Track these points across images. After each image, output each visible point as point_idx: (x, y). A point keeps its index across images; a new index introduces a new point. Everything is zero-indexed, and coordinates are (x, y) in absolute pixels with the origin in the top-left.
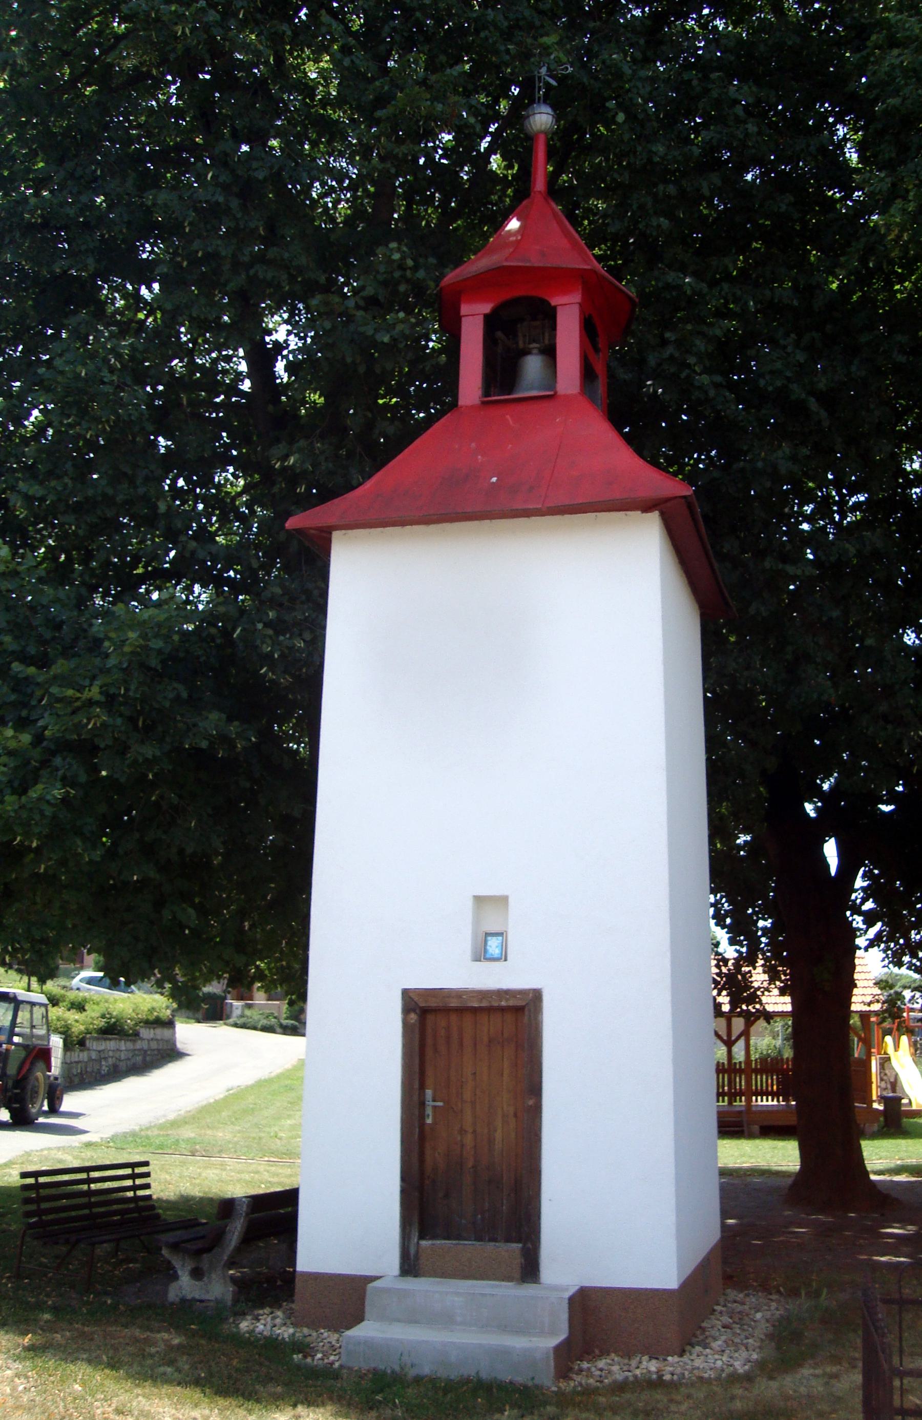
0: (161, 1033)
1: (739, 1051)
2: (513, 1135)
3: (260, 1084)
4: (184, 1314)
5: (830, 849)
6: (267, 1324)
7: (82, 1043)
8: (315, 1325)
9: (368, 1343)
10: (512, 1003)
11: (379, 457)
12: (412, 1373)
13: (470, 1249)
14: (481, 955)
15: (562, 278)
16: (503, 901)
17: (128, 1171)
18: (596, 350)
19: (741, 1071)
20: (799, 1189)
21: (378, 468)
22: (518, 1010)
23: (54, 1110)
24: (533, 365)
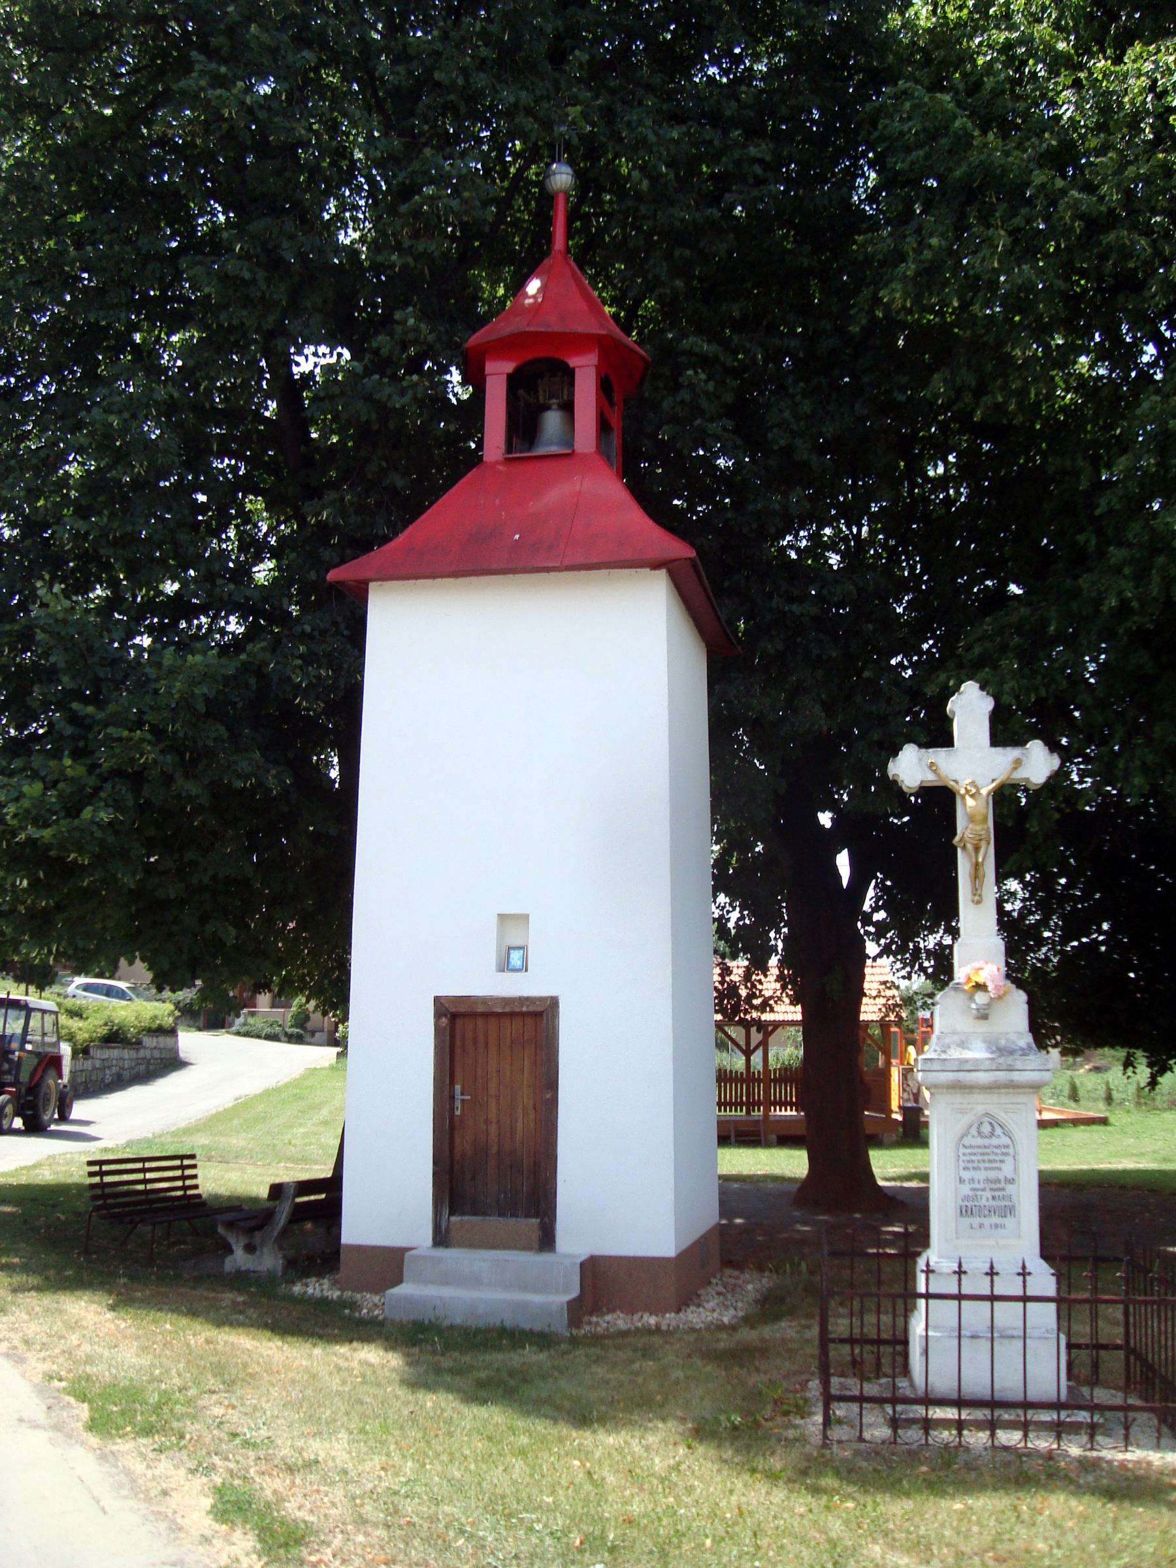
0: (163, 1041)
1: (757, 1058)
2: (532, 1124)
3: (267, 1093)
4: (240, 1280)
5: (843, 861)
6: (316, 1288)
7: (86, 1051)
8: (359, 1289)
9: (408, 1299)
10: (531, 1009)
11: (411, 507)
12: (446, 1323)
13: (494, 1224)
14: (504, 966)
15: (581, 342)
16: (525, 918)
17: (177, 1163)
18: (612, 404)
19: (759, 1081)
20: (806, 1193)
21: (407, 523)
22: (537, 1015)
23: (64, 1118)
24: (552, 420)
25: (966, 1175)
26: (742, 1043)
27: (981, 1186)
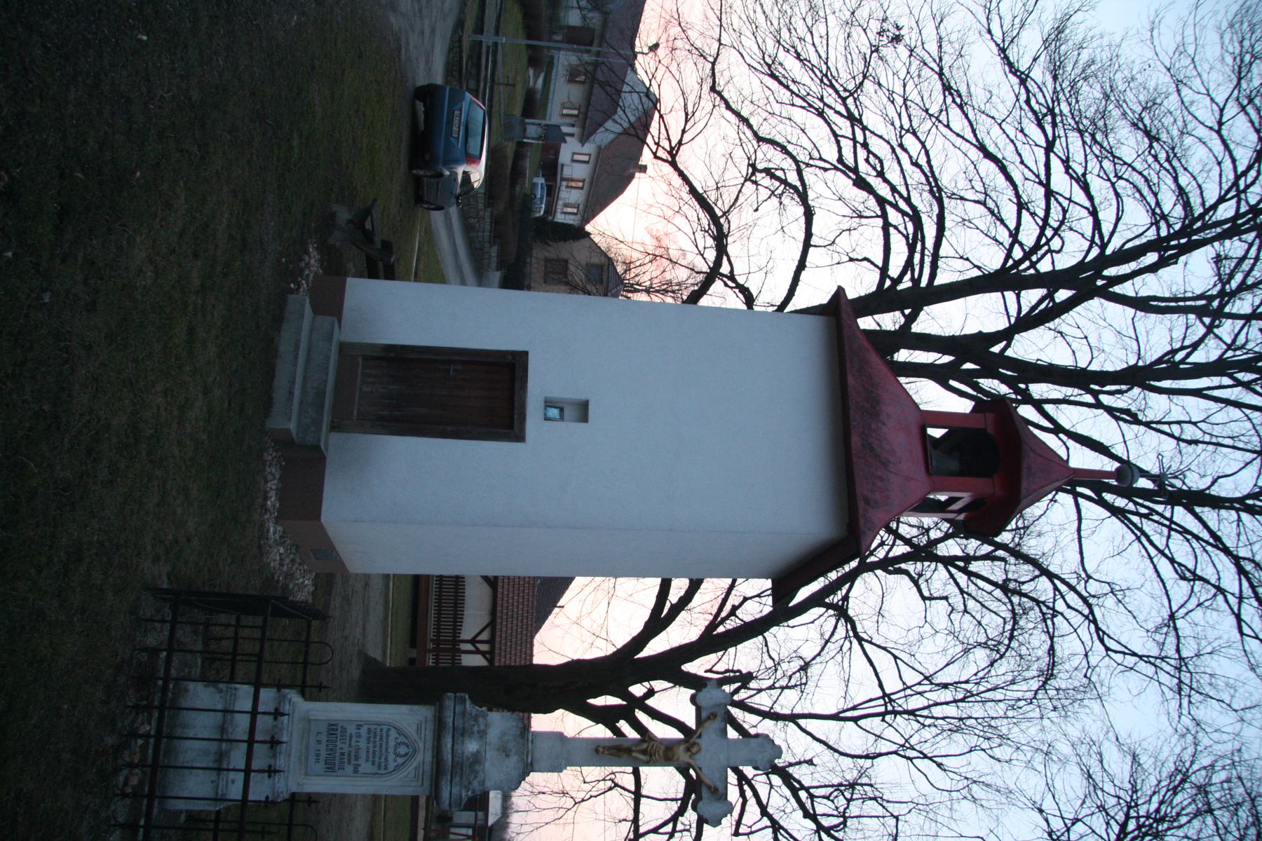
10: (516, 422)
14: (549, 404)
22: (511, 427)
25: (363, 731)
26: (479, 638)
27: (353, 744)
